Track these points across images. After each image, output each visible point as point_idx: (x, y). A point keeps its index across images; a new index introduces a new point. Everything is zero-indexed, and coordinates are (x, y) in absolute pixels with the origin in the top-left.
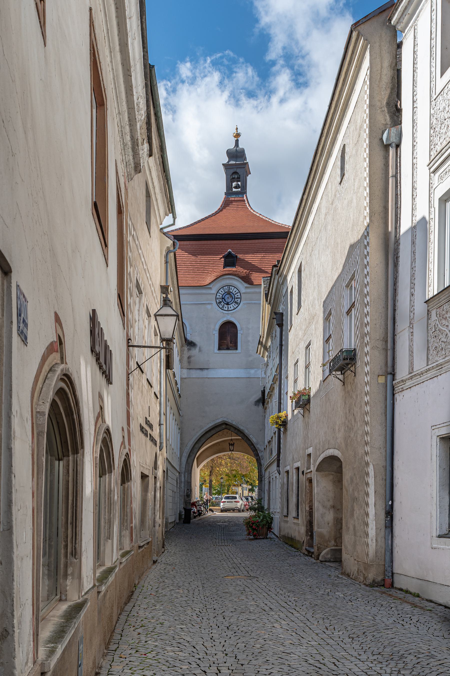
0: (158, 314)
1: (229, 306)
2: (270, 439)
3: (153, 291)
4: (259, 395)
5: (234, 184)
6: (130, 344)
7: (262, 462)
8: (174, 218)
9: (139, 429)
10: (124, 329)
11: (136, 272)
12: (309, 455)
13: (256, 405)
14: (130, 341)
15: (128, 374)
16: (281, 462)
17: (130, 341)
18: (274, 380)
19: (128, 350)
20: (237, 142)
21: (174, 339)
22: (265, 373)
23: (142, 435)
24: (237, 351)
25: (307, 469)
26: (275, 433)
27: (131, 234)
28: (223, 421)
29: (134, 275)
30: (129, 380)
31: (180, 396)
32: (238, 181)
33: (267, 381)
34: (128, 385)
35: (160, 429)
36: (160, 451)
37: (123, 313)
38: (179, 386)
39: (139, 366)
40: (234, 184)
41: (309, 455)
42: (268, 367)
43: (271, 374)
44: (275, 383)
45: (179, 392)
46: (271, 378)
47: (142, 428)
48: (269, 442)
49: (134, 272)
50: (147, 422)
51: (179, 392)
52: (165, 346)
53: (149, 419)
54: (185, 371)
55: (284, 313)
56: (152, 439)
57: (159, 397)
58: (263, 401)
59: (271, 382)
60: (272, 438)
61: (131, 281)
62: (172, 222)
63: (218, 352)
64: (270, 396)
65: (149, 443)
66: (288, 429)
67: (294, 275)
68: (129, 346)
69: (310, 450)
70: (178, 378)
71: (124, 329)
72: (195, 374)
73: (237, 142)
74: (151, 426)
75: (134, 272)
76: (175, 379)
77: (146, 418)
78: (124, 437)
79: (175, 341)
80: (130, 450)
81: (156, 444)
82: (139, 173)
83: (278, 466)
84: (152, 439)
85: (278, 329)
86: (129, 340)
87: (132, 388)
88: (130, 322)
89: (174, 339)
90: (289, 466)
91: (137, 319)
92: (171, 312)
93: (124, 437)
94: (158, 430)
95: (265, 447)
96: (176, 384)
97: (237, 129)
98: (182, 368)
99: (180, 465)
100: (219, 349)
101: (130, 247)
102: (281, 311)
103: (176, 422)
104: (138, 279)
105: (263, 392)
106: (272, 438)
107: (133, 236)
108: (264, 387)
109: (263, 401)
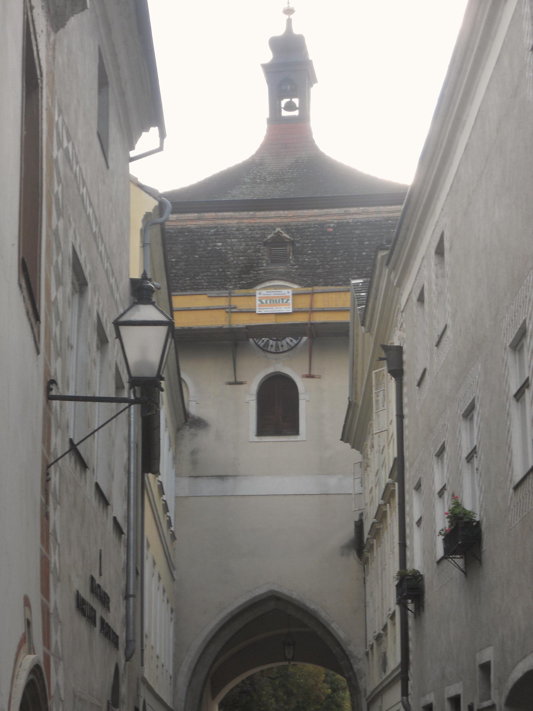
0: (125, 318)
1: (279, 343)
2: (378, 629)
3: (114, 286)
4: (349, 531)
5: (284, 102)
6: (53, 393)
7: (362, 683)
8: (162, 135)
9: (73, 604)
10: (38, 352)
11: (71, 233)
12: (486, 668)
13: (342, 554)
14: (53, 386)
15: (47, 467)
16: (410, 683)
17: (53, 386)
18: (387, 495)
19: (48, 408)
20: (289, 22)
21: (162, 379)
22: (362, 483)
23: (80, 624)
24: (298, 438)
25: (482, 700)
26: (392, 617)
27: (60, 144)
28: (271, 591)
29: (66, 236)
30: (48, 480)
31: (173, 537)
32: (292, 97)
33: (368, 501)
34: (46, 491)
35: (127, 608)
36: (127, 660)
37: (34, 314)
38: (171, 514)
39: (73, 447)
40: (284, 102)
41: (486, 668)
42: (369, 469)
43: (378, 483)
44: (389, 502)
45: (172, 529)
46: (378, 493)
47: (81, 605)
48: (378, 638)
49: (66, 231)
50: (95, 589)
51: (172, 529)
52: (138, 395)
53: (98, 581)
54: (185, 482)
55: (405, 348)
56: (107, 632)
57: (125, 530)
58: (360, 545)
59: (378, 501)
60: (385, 628)
61: (59, 247)
62: (158, 146)
63: (257, 439)
64: (376, 532)
65: (99, 640)
66: (426, 604)
67: (425, 262)
68: (50, 398)
69: (488, 655)
70: (169, 497)
71: (38, 352)
72: (208, 487)
73: (289, 22)
74: (104, 600)
75: (66, 231)
76: (164, 497)
77: (92, 579)
78: (28, 623)
79: (163, 384)
80: (47, 659)
81: (116, 644)
82: (83, 10)
83: (405, 693)
84: (107, 632)
85: (392, 383)
86: (50, 383)
87: (58, 502)
88: (55, 342)
89: (162, 379)
90: (432, 694)
91: (74, 343)
92: (157, 316)
93: (28, 623)
94: (123, 610)
95: (368, 649)
96: (166, 508)
97: (288, 3)
98: (178, 475)
99: (174, 694)
100: (261, 431)
101: (58, 173)
102: (397, 343)
103: (166, 595)
104: (77, 250)
105: (359, 526)
106: (385, 628)
107: (66, 152)
108: (361, 515)
109: (360, 545)
